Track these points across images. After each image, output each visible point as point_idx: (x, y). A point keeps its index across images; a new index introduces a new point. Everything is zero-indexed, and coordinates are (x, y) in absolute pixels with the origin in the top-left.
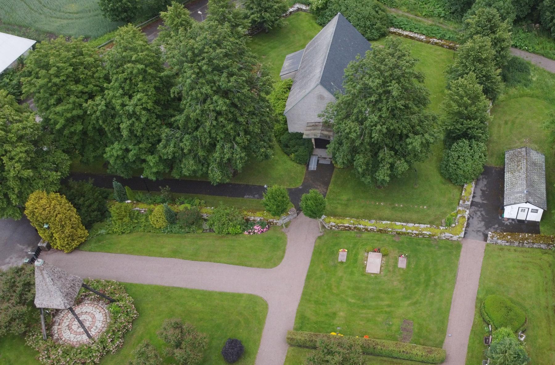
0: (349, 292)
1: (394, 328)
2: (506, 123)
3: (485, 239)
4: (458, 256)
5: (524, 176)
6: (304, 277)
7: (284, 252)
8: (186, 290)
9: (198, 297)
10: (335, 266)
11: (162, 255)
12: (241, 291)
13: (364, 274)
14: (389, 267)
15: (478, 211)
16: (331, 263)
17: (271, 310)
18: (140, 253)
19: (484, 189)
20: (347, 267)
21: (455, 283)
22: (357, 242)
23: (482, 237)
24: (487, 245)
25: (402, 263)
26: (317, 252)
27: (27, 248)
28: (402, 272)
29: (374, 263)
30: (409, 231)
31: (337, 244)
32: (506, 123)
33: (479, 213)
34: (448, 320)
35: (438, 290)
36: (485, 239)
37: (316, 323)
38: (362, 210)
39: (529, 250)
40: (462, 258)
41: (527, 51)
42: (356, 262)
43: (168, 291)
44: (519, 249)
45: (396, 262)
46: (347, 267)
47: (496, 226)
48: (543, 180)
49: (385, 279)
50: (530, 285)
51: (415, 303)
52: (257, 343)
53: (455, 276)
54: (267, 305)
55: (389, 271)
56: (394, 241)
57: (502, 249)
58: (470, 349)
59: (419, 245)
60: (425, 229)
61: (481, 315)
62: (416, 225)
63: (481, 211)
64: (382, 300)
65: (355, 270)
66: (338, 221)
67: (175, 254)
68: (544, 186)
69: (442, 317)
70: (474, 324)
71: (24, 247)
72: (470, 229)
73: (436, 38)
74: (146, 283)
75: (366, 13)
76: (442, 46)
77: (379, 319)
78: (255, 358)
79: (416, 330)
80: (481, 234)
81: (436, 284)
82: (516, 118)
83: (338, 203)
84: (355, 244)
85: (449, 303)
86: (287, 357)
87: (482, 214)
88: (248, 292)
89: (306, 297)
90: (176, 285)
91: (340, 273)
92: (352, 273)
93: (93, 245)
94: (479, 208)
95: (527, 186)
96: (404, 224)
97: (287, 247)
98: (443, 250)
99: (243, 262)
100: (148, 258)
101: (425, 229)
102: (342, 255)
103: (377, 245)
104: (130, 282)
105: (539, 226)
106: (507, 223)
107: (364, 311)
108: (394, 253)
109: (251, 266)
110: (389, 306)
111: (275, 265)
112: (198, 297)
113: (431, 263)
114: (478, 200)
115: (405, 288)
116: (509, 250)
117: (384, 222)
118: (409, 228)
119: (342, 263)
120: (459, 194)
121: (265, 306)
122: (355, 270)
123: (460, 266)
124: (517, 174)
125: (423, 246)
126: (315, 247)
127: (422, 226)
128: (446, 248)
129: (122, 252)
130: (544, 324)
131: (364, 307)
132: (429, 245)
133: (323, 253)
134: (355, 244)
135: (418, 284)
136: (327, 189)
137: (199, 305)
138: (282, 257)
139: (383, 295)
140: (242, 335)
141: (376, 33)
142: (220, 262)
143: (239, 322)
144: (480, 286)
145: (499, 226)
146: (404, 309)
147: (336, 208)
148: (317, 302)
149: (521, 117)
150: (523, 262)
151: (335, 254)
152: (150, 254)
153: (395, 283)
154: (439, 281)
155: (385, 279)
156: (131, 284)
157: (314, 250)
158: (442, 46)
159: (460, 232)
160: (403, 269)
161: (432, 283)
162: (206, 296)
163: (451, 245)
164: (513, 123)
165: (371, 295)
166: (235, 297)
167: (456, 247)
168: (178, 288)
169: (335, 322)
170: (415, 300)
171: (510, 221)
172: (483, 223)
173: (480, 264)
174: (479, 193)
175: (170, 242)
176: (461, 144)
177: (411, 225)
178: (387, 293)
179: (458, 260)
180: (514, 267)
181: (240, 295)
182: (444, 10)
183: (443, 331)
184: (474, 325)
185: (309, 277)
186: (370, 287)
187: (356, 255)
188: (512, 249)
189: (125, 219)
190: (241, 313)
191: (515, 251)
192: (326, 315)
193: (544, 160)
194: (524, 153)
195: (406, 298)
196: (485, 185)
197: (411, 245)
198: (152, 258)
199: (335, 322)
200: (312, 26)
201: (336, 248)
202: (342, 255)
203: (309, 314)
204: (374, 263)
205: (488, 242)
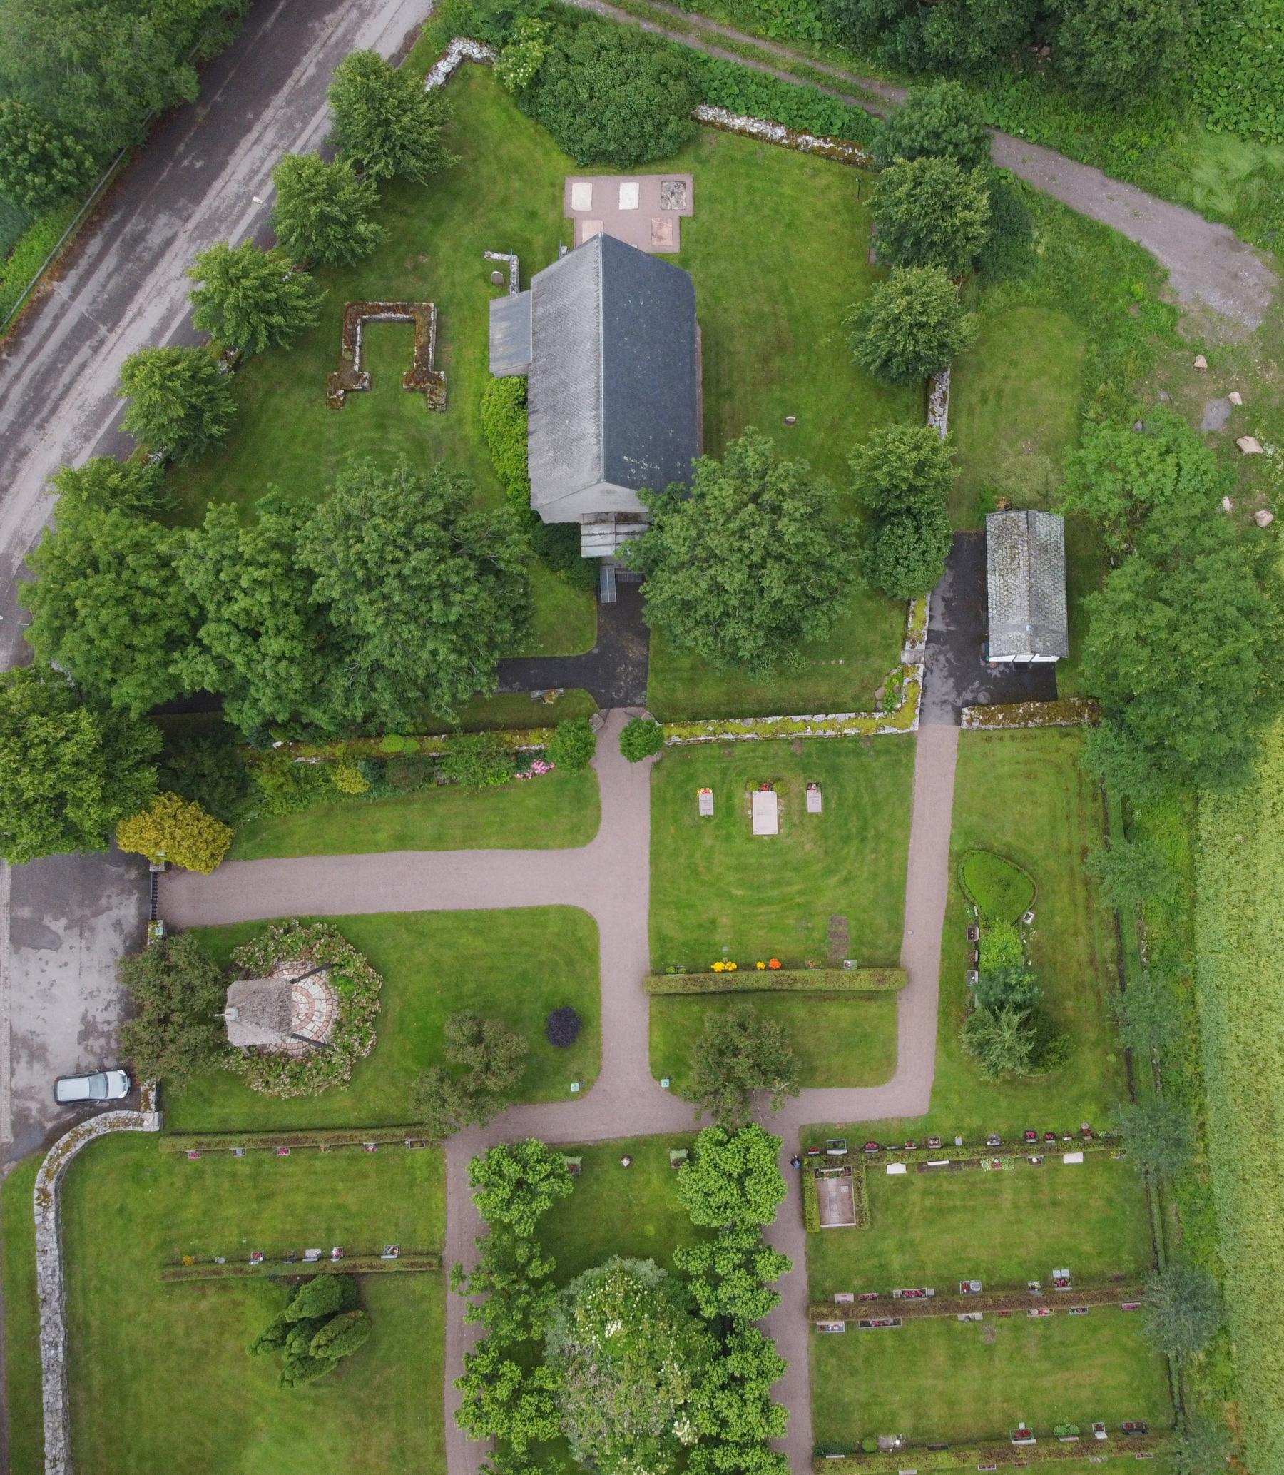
0: (732, 877)
1: (817, 935)
2: (984, 400)
3: (958, 722)
4: (910, 767)
5: (1025, 587)
6: (646, 859)
7: (599, 808)
8: (446, 914)
9: (472, 924)
10: (697, 827)
11: (378, 847)
12: (543, 902)
13: (751, 838)
14: (792, 815)
15: (940, 652)
16: (688, 821)
17: (604, 930)
18: (336, 848)
19: (949, 595)
20: (718, 826)
21: (909, 827)
22: (727, 768)
23: (950, 717)
24: (963, 733)
25: (814, 801)
26: (658, 800)
27: (127, 871)
28: (816, 821)
29: (765, 813)
30: (819, 732)
31: (691, 778)
32: (984, 400)
33: (942, 658)
34: (903, 902)
35: (883, 846)
36: (958, 722)
37: (684, 945)
38: (724, 688)
39: (1038, 732)
40: (918, 771)
41: (1025, 137)
42: (732, 815)
43: (416, 922)
44: (1019, 734)
45: (804, 804)
46: (718, 826)
47: (977, 684)
48: (1062, 586)
49: (790, 841)
50: (1040, 811)
51: (846, 881)
52: (596, 998)
53: (909, 810)
54: (594, 922)
55: (794, 825)
56: (793, 755)
57: (988, 739)
58: (946, 953)
59: (839, 755)
60: (848, 723)
61: (959, 886)
62: (831, 717)
63: (945, 653)
64: (789, 883)
65: (734, 831)
66: (684, 732)
67: (402, 841)
68: (1062, 598)
69: (893, 895)
70: (949, 906)
71: (121, 870)
72: (928, 700)
73: (811, 134)
74: (372, 912)
75: (639, 103)
76: (828, 156)
77: (791, 921)
78: (599, 1025)
79: (854, 933)
80: (949, 708)
81: (878, 835)
82: (1005, 378)
83: (675, 679)
84: (724, 773)
85: (903, 869)
86: (651, 1017)
87: (948, 660)
88: (556, 901)
89: (659, 897)
90: (427, 907)
91: (708, 841)
92: (729, 838)
93: (245, 845)
94: (943, 644)
95: (1032, 614)
96: (807, 717)
97: (601, 796)
98: (883, 759)
99: (529, 839)
100: (356, 857)
101: (848, 723)
102: (706, 803)
103: (765, 772)
104: (344, 912)
105: (1053, 672)
106: (995, 673)
107: (761, 910)
108: (796, 783)
109: (547, 847)
110: (802, 893)
111: (590, 838)
112: (472, 924)
113: (862, 787)
114: (939, 625)
115: (826, 853)
116: (1001, 739)
117: (770, 720)
118: (818, 725)
119: (708, 818)
120: (901, 621)
121: (593, 924)
122: (734, 831)
123: (916, 788)
124: (1010, 579)
125: (847, 755)
126: (652, 787)
127: (842, 717)
128: (888, 752)
129: (305, 852)
130: (1064, 886)
131: (761, 902)
132: (858, 753)
133: (670, 801)
134: (724, 773)
135: (846, 840)
136: (647, 646)
137: (479, 942)
138: (599, 819)
139: (789, 874)
140: (567, 986)
141: (670, 147)
142: (489, 847)
143: (557, 964)
144: (953, 826)
145: (982, 684)
146: (831, 894)
147: (674, 691)
148: (677, 905)
149: (1014, 373)
150: (1026, 762)
151: (692, 800)
152: (356, 847)
153: (808, 847)
154: (883, 827)
155: (790, 841)
156: (346, 917)
157: (652, 795)
158: (828, 156)
159: (911, 719)
160: (816, 815)
161: (871, 833)
162: (483, 921)
163: (897, 745)
164: (999, 394)
165: (769, 877)
166: (536, 915)
167: (907, 744)
168: (432, 912)
169: (717, 937)
170: (845, 873)
171: (1001, 668)
172: (951, 681)
173: (951, 778)
174: (940, 607)
175: (387, 819)
176: (900, 531)
177: (820, 718)
178: (796, 869)
179: (911, 775)
180: (1012, 776)
181: (544, 911)
182: (818, 18)
183: (897, 927)
184: (949, 906)
185: (655, 856)
186: (764, 861)
187: (730, 797)
188: (1007, 734)
189: (285, 788)
190: (555, 947)
191: (1013, 738)
192: (700, 926)
193: (1061, 529)
194: (1023, 526)
195: (831, 872)
196: (951, 585)
197: (824, 762)
198: (364, 857)
199: (717, 937)
200: (510, 118)
201: (690, 787)
202: (706, 803)
203: (670, 929)
204: (765, 813)
205: (965, 725)
